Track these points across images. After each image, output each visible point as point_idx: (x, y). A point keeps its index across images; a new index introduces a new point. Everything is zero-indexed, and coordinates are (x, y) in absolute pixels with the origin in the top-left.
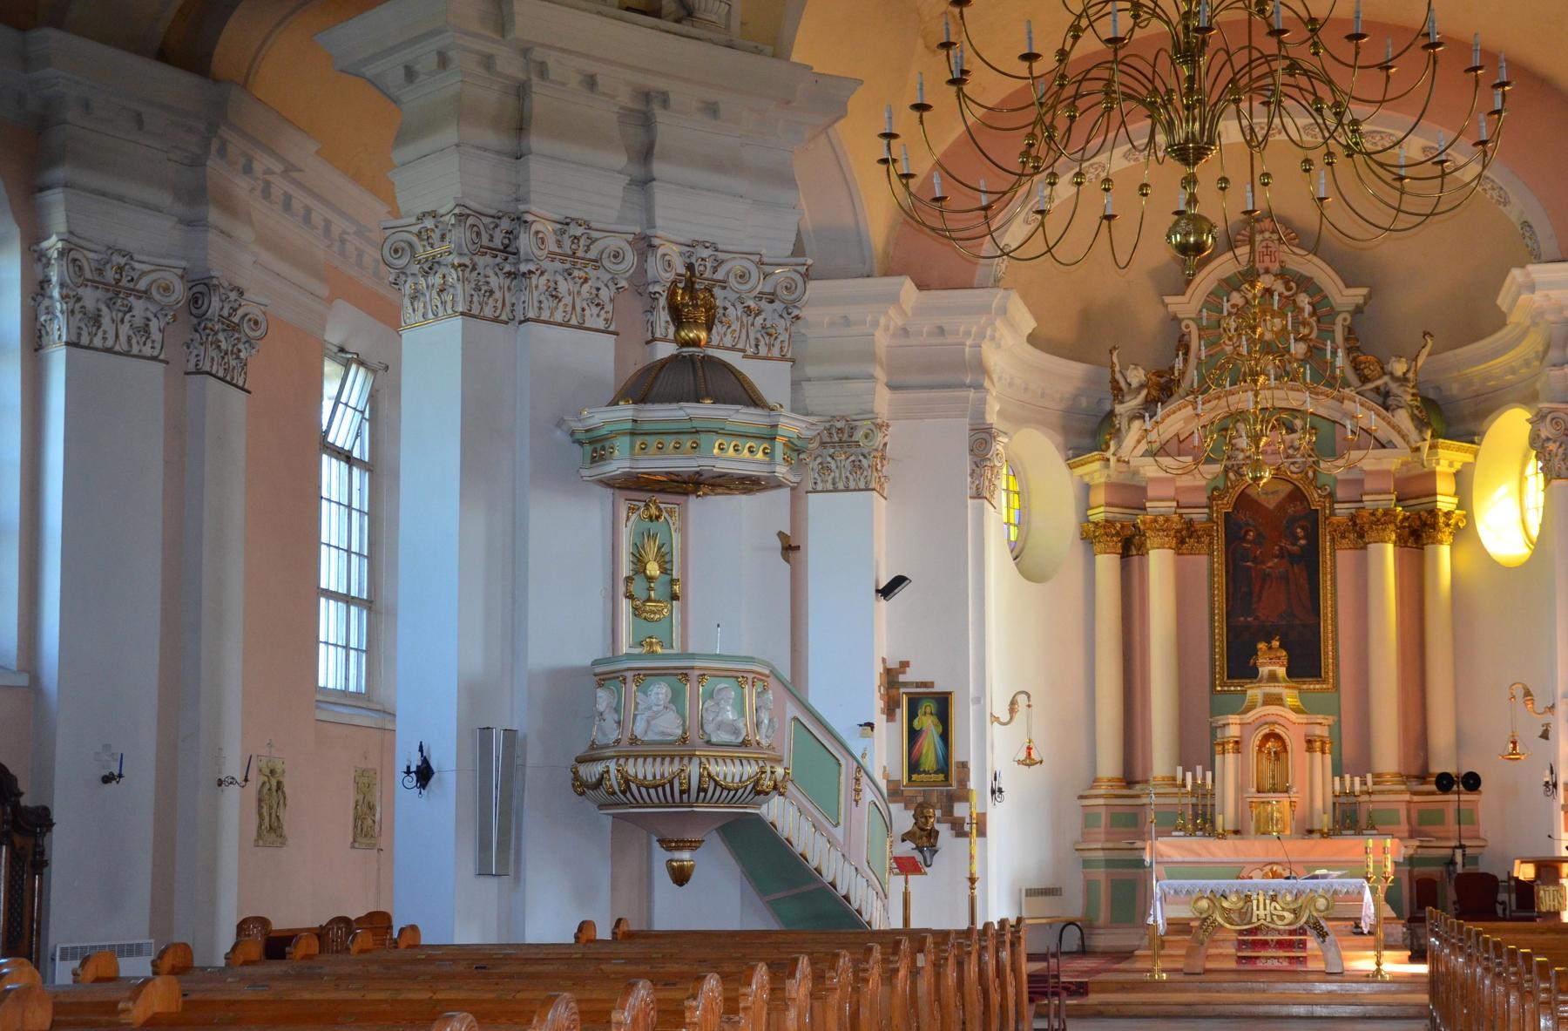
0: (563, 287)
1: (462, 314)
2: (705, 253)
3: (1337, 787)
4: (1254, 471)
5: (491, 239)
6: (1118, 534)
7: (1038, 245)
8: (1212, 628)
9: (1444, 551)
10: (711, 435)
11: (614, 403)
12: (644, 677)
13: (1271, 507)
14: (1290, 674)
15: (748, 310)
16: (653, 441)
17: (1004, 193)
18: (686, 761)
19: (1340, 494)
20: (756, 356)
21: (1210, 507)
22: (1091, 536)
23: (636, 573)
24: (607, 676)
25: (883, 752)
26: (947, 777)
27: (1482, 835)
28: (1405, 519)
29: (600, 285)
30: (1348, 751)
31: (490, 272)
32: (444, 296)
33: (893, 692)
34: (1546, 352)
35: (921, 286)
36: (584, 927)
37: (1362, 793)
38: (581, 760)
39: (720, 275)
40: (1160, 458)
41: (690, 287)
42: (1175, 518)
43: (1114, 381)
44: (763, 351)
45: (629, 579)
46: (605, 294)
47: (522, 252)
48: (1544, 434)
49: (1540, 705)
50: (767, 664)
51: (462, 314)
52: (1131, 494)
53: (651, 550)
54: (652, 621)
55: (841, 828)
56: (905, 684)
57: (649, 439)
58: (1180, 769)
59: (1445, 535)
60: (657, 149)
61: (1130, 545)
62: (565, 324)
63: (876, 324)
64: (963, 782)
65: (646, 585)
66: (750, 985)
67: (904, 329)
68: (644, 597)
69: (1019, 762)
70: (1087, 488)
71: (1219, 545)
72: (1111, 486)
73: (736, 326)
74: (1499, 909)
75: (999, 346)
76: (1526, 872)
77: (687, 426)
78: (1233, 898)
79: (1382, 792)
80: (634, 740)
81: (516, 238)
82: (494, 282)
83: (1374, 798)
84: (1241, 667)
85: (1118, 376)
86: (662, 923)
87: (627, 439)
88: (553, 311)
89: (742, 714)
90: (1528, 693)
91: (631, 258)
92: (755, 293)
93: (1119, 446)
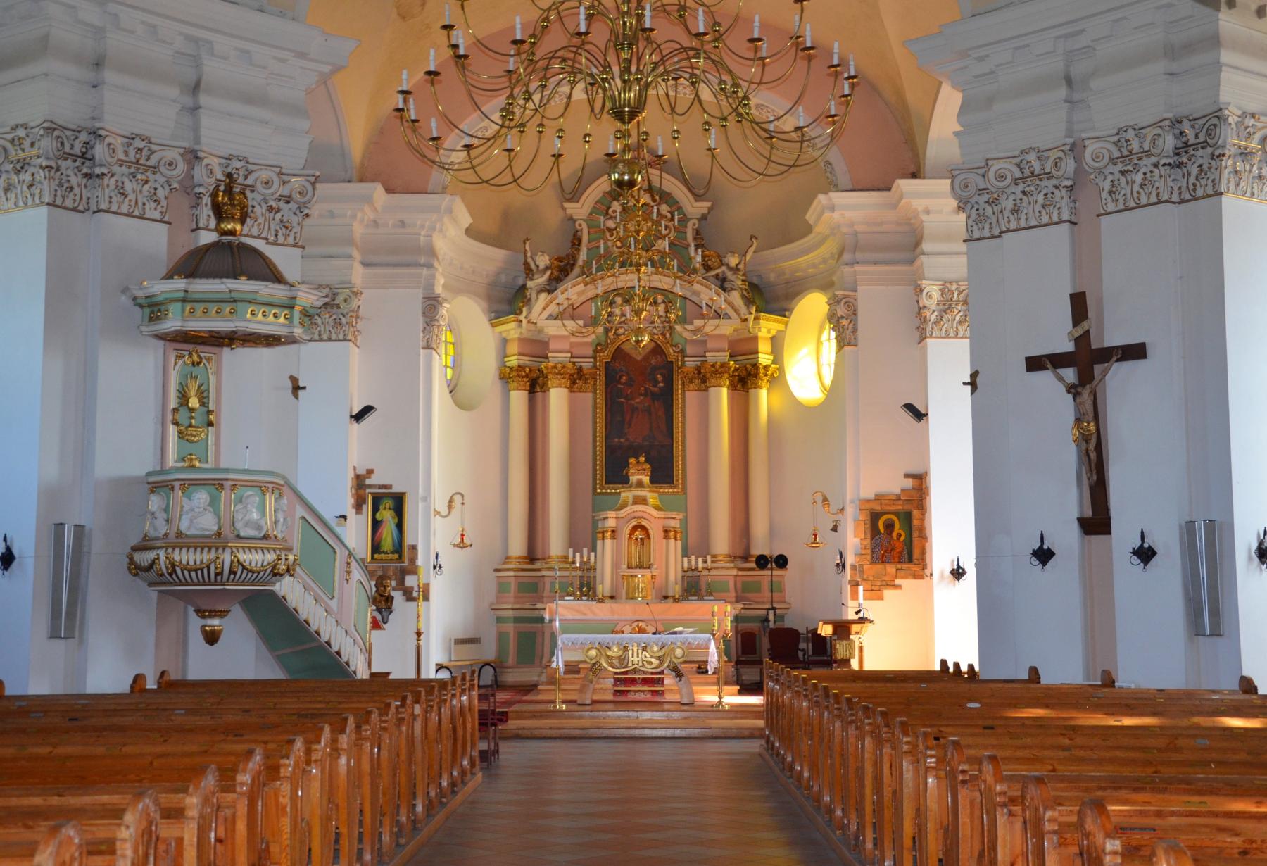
0: (129, 186)
1: (48, 204)
2: (239, 164)
3: (686, 565)
4: (637, 336)
5: (72, 147)
6: (527, 376)
7: (507, 178)
8: (595, 447)
9: (763, 394)
10: (247, 304)
11: (169, 276)
12: (188, 485)
13: (639, 358)
14: (652, 481)
15: (271, 209)
16: (200, 307)
17: (489, 139)
18: (220, 550)
19: (689, 351)
20: (275, 243)
21: (595, 358)
22: (507, 377)
23: (181, 405)
24: (158, 484)
25: (355, 534)
26: (400, 557)
27: (787, 599)
28: (736, 370)
29: (157, 186)
30: (693, 538)
31: (70, 172)
32: (33, 189)
33: (361, 492)
34: (841, 253)
35: (389, 190)
36: (138, 679)
37: (704, 569)
38: (135, 549)
39: (249, 181)
40: (555, 321)
41: (229, 191)
42: (570, 365)
43: (526, 264)
44: (281, 239)
45: (175, 410)
46: (161, 193)
47: (97, 157)
48: (839, 313)
49: (834, 508)
50: (283, 477)
51: (48, 204)
52: (537, 347)
53: (193, 388)
54: (192, 442)
55: (335, 600)
56: (370, 486)
57: (196, 305)
58: (571, 551)
59: (764, 382)
60: (203, 86)
61: (535, 384)
62: (130, 215)
63: (354, 217)
64: (413, 560)
65: (188, 414)
66: (319, 742)
67: (375, 222)
68: (186, 423)
69: (455, 545)
70: (505, 342)
71: (600, 386)
72: (523, 341)
73: (261, 220)
74: (800, 654)
75: (445, 237)
76: (826, 630)
77: (227, 296)
78: (615, 649)
79: (716, 569)
80: (179, 534)
81: (92, 148)
82: (74, 181)
83: (712, 573)
84: (615, 473)
85: (529, 260)
86: (194, 674)
87: (179, 305)
88: (120, 204)
89: (264, 514)
90: (825, 499)
91: (181, 167)
92: (276, 196)
93: (529, 312)
